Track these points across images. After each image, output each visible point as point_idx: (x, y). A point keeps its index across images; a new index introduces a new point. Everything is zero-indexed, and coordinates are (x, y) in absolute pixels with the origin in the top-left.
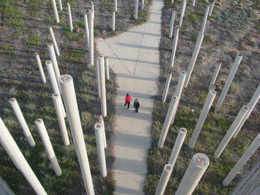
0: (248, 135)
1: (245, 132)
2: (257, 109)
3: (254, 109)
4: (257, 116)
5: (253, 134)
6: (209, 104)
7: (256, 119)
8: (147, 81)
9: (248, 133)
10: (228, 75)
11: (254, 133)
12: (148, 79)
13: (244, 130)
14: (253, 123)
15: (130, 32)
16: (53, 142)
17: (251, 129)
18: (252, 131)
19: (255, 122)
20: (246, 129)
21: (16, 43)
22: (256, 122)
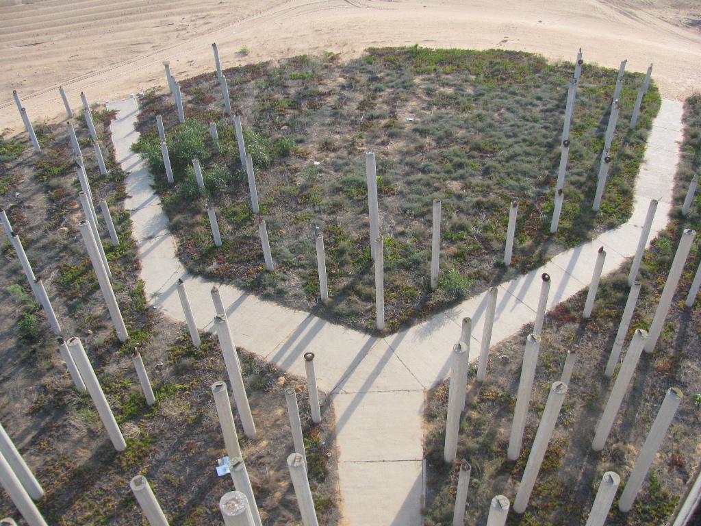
0: (79, 518)
1: (69, 520)
2: (37, 455)
3: (30, 463)
4: (54, 468)
5: (83, 506)
6: (119, 438)
7: (57, 475)
8: (635, 206)
9: (74, 514)
10: (97, 294)
11: (83, 500)
12: (515, 306)
13: (62, 520)
14: (63, 488)
15: (346, 417)
16: (592, 194)
17: (71, 503)
18: (77, 503)
19: (62, 480)
20: (64, 513)
21: (503, 161)
22: (65, 480)
